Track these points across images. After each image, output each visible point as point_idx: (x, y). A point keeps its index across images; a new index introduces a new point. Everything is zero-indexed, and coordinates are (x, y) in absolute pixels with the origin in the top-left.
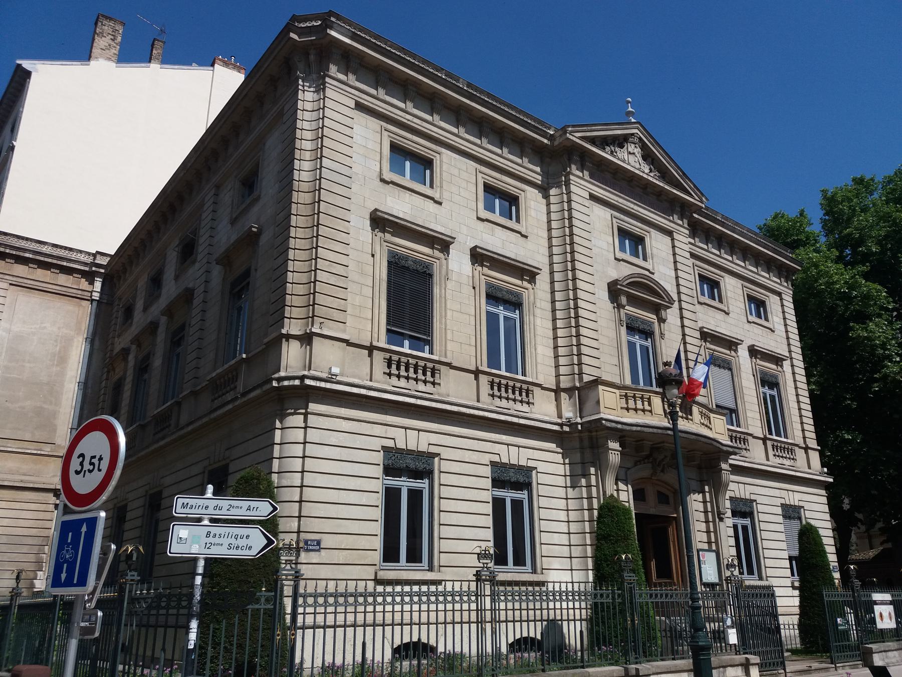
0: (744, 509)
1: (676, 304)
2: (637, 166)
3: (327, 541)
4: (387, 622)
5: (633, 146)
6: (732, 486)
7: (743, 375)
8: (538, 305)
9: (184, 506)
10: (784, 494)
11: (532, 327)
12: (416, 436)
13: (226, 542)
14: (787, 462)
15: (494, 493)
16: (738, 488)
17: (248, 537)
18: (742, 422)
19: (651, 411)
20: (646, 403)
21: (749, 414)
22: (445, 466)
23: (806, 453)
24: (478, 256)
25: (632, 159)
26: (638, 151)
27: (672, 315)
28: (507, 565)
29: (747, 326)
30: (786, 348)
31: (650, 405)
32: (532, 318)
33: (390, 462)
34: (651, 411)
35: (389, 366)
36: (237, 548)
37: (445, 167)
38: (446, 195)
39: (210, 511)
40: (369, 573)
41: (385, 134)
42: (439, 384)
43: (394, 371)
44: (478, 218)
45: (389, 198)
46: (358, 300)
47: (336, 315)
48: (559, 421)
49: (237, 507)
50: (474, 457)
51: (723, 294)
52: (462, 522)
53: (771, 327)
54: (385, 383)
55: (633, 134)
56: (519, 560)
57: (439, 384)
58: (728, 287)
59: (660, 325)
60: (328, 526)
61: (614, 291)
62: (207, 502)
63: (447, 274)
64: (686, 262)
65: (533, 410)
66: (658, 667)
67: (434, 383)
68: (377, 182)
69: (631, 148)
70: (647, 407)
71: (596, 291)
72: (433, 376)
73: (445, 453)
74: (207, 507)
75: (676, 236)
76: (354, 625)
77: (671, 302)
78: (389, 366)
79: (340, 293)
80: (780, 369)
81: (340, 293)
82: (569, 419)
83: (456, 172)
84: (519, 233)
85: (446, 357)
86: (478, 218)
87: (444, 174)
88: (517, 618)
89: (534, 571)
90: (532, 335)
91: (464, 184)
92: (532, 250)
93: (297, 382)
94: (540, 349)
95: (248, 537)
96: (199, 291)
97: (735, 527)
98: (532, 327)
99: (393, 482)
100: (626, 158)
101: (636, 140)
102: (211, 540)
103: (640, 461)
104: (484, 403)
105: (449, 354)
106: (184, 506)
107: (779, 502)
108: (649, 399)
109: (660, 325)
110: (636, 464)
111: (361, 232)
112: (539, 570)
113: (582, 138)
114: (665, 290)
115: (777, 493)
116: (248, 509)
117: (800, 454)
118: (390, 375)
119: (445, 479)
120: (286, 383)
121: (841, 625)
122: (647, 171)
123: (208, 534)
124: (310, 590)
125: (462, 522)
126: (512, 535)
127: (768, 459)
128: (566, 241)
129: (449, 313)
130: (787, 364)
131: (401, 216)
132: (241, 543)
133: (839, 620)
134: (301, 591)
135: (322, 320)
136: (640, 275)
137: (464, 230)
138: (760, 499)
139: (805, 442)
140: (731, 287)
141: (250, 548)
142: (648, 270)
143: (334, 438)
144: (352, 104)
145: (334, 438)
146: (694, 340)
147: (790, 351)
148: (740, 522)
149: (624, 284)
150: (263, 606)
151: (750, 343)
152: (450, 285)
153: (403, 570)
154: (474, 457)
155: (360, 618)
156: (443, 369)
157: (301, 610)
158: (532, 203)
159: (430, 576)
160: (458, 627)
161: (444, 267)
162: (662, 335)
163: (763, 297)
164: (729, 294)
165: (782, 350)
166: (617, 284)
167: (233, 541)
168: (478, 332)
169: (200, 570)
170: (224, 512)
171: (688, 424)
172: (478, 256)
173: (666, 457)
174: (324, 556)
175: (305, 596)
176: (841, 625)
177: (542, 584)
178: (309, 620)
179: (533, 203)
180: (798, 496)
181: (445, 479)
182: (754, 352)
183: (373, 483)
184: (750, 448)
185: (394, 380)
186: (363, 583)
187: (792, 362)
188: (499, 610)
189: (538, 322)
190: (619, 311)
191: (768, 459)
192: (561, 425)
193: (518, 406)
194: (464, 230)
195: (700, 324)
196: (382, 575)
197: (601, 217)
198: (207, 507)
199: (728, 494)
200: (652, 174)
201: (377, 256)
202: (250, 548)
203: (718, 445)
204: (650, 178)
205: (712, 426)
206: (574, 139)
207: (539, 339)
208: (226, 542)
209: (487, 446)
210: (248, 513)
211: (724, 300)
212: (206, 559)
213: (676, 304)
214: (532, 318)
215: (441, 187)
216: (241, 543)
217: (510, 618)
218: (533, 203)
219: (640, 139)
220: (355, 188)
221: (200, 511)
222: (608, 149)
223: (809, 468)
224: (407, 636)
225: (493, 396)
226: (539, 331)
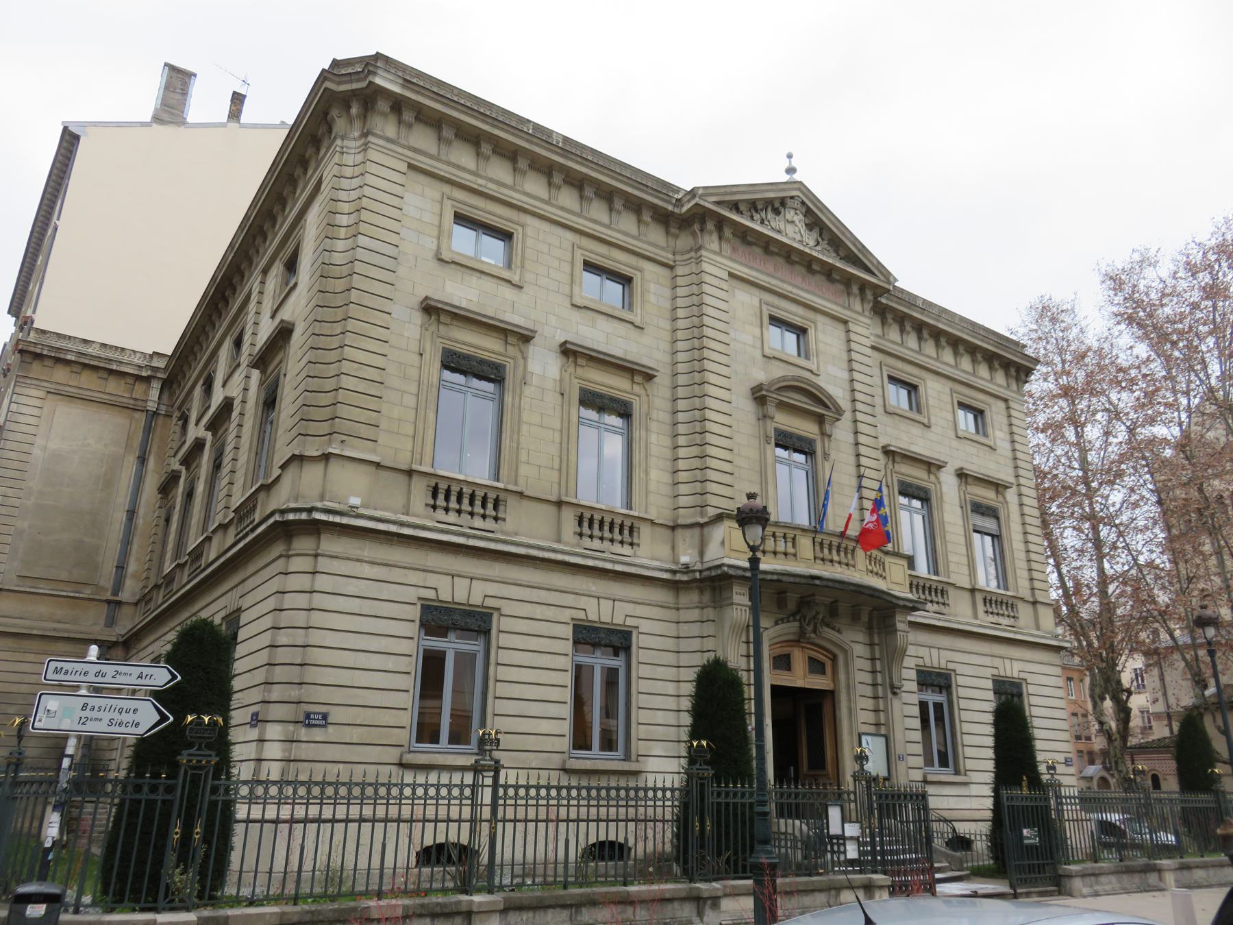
0: (936, 681)
1: (848, 416)
2: (798, 237)
3: (336, 715)
4: (529, 817)
5: (792, 212)
6: (911, 650)
7: (946, 507)
8: (654, 416)
9: (57, 671)
10: (997, 662)
11: (643, 445)
12: (464, 586)
13: (107, 716)
14: (1004, 621)
15: (576, 658)
16: (921, 652)
17: (135, 711)
18: (941, 569)
19: (795, 555)
20: (790, 544)
21: (952, 558)
22: (506, 624)
23: (1035, 611)
24: (568, 351)
25: (790, 229)
26: (799, 218)
27: (842, 432)
28: (590, 749)
29: (955, 443)
30: (1011, 471)
31: (794, 546)
32: (643, 433)
33: (430, 617)
34: (795, 555)
35: (435, 496)
36: (120, 724)
37: (529, 242)
38: (529, 277)
39: (91, 678)
40: (392, 755)
41: (448, 203)
42: (504, 520)
43: (441, 501)
44: (573, 305)
45: (448, 283)
46: (396, 412)
47: (365, 431)
48: (674, 567)
49: (126, 674)
50: (550, 613)
51: (923, 401)
52: (529, 695)
53: (992, 444)
54: (426, 517)
55: (792, 198)
56: (608, 743)
57: (504, 520)
58: (930, 392)
59: (823, 442)
60: (337, 696)
61: (759, 396)
62: (86, 667)
63: (524, 377)
64: (868, 362)
65: (639, 553)
66: (733, 887)
67: (496, 519)
68: (433, 265)
69: (790, 215)
70: (791, 550)
71: (733, 398)
72: (496, 508)
73: (507, 608)
74: (86, 673)
75: (852, 326)
76: (547, 821)
77: (839, 412)
78: (435, 496)
79: (372, 403)
80: (1001, 498)
81: (372, 403)
82: (687, 566)
83: (545, 248)
84: (632, 323)
85: (516, 484)
86: (573, 305)
87: (528, 251)
88: (553, 817)
89: (627, 758)
90: (643, 455)
91: (556, 264)
92: (646, 346)
93: (304, 516)
94: (654, 474)
95: (135, 711)
96: (237, 403)
97: (923, 706)
98: (643, 445)
99: (435, 643)
100: (782, 227)
101: (796, 204)
102: (87, 713)
103: (782, 619)
104: (567, 544)
105: (521, 481)
106: (57, 671)
107: (989, 672)
108: (794, 539)
109: (823, 442)
110: (776, 623)
111: (408, 328)
112: (633, 757)
113: (718, 203)
114: (830, 397)
115: (987, 661)
116: (140, 677)
117: (1024, 611)
118: (434, 507)
119: (504, 640)
120: (291, 517)
121: (1029, 838)
122: (812, 243)
123: (85, 707)
124: (512, 781)
125: (529, 695)
126: (598, 714)
127: (976, 617)
128: (693, 336)
129: (524, 428)
130: (1011, 495)
131: (463, 305)
132: (126, 718)
133: (1025, 832)
134: (502, 781)
135: (344, 437)
136: (794, 378)
137: (553, 320)
138: (960, 669)
139: (1033, 595)
140: (935, 391)
141: (137, 725)
142: (811, 371)
143: (352, 587)
144: (403, 167)
145: (352, 587)
146: (874, 462)
147: (1017, 476)
148: (932, 697)
149: (773, 389)
150: (221, 798)
151: (958, 464)
152: (528, 391)
153: (596, 758)
154: (550, 613)
155: (442, 812)
156: (511, 501)
157: (501, 802)
158: (652, 287)
159: (626, 766)
160: (552, 826)
161: (521, 368)
162: (826, 456)
163: (981, 406)
164: (931, 402)
165: (1005, 475)
166: (761, 389)
167: (116, 716)
168: (564, 452)
169: (70, 750)
170: (108, 679)
171: (847, 572)
172: (568, 351)
173: (818, 613)
174: (332, 733)
175: (506, 787)
176: (1029, 838)
177: (636, 773)
178: (510, 814)
179: (653, 286)
180: (1017, 666)
181: (504, 640)
182: (962, 475)
183: (404, 644)
184: (951, 602)
185: (440, 515)
186: (544, 774)
187: (1019, 490)
188: (481, 805)
189: (653, 438)
190: (765, 425)
191: (976, 617)
192: (674, 572)
193: (617, 548)
194: (553, 320)
195: (883, 441)
196: (409, 758)
197: (745, 302)
198: (86, 673)
199: (909, 662)
200: (819, 248)
201: (427, 356)
202: (137, 725)
203: (889, 598)
204: (815, 254)
205: (887, 574)
206: (707, 205)
207: (653, 461)
208: (107, 716)
209: (569, 600)
210: (140, 681)
211: (925, 411)
212: (79, 738)
213: (848, 416)
214: (643, 433)
215: (523, 267)
216: (126, 718)
217: (553, 816)
218: (653, 286)
219: (803, 203)
220: (401, 271)
221: (77, 678)
222: (757, 217)
223: (1038, 628)
224: (429, 836)
225: (581, 535)
226: (654, 450)
